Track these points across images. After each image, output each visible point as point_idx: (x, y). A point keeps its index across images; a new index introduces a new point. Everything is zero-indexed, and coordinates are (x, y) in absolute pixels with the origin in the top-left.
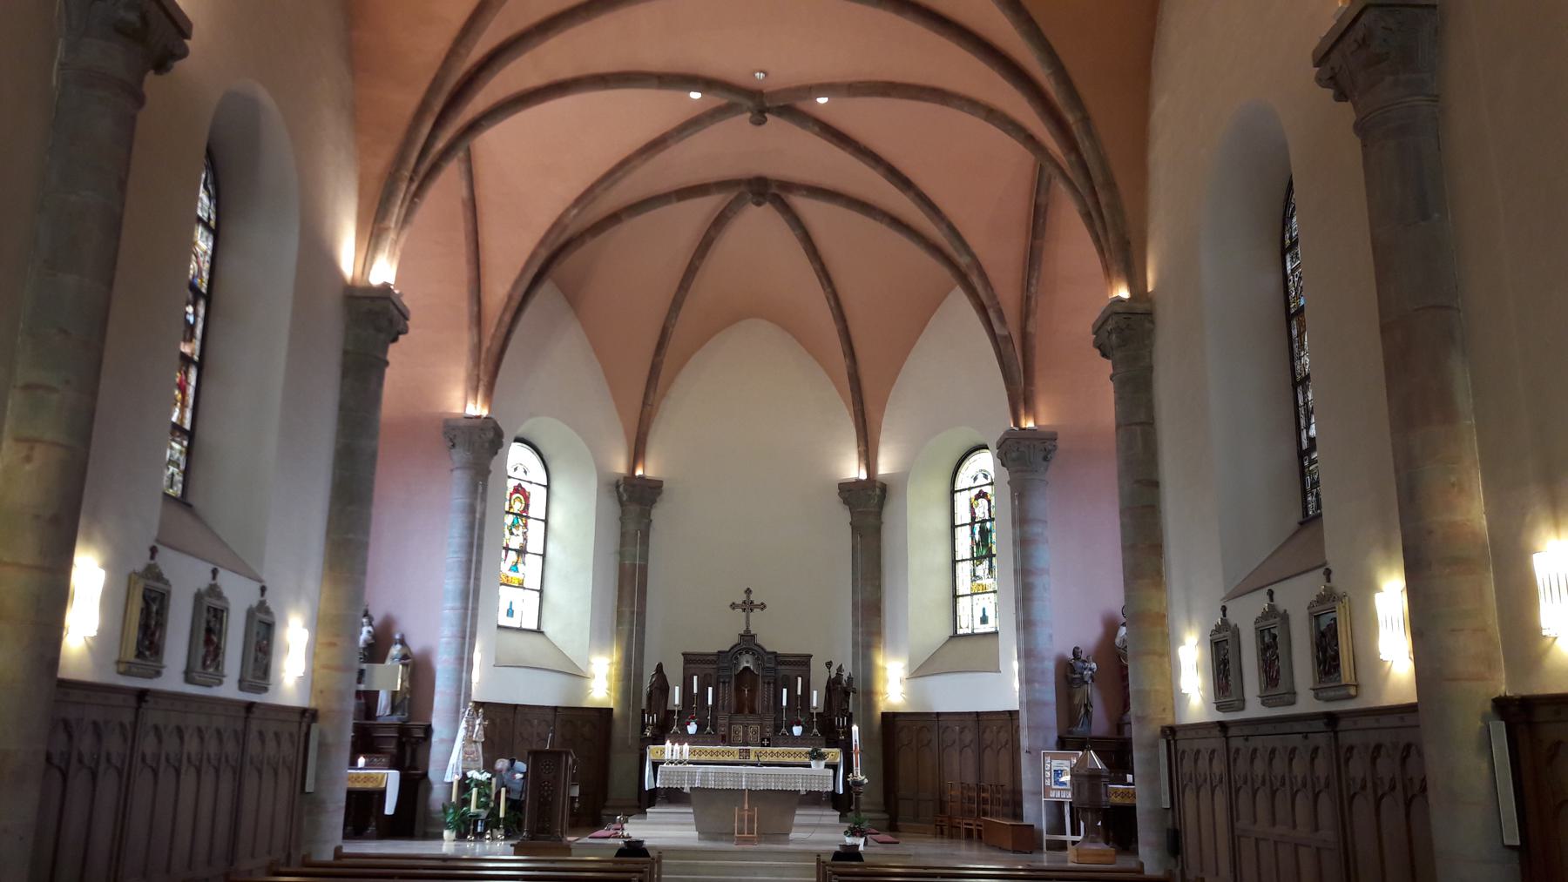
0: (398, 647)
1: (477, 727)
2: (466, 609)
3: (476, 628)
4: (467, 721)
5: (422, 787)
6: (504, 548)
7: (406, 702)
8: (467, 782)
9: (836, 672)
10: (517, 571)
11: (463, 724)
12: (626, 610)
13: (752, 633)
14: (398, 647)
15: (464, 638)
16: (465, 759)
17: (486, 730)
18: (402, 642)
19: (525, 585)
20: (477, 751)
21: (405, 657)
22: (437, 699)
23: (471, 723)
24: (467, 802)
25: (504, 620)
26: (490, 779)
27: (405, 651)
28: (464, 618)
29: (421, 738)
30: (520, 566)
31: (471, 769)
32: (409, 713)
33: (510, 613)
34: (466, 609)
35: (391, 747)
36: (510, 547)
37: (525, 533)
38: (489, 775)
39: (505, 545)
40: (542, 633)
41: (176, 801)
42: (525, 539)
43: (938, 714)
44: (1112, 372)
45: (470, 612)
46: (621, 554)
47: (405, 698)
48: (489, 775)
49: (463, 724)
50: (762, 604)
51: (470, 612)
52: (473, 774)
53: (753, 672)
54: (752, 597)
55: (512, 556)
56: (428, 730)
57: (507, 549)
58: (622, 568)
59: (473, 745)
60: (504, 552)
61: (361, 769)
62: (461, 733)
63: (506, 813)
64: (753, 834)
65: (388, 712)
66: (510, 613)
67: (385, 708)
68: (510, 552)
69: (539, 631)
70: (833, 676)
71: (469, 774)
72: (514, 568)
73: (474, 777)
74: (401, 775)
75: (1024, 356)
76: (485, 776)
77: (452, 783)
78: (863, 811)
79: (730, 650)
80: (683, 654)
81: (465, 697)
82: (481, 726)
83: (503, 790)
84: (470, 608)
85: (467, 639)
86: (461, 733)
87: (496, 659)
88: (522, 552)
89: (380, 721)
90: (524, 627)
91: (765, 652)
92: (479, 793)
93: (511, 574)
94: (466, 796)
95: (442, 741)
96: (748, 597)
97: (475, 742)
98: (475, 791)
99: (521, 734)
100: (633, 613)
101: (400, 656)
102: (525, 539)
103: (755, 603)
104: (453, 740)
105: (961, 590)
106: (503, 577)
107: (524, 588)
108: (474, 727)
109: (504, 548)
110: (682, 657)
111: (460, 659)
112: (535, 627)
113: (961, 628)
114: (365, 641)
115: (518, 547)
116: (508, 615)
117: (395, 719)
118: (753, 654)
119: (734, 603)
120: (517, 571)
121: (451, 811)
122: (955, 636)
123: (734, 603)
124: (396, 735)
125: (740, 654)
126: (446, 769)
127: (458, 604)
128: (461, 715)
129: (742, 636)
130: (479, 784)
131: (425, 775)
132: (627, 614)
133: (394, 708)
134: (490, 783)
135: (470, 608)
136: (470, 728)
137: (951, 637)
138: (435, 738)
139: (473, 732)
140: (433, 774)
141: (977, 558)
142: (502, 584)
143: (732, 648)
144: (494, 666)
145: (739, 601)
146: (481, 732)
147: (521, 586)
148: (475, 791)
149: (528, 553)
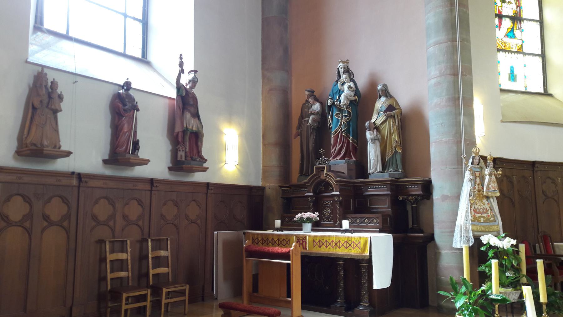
0: (383, 99)
1: (487, 178)
2: (454, 40)
3: (470, 62)
4: (473, 173)
5: (430, 253)
6: (497, 15)
7: (398, 158)
8: (482, 249)
10: (514, 37)
11: (468, 175)
14: (383, 99)
15: (455, 75)
16: (475, 220)
17: (499, 181)
18: (386, 93)
19: (525, 50)
20: (491, 209)
21: (390, 108)
22: (433, 149)
23: (478, 174)
24: (484, 277)
25: (507, 85)
26: (517, 246)
27: (390, 102)
28: (453, 50)
29: (418, 195)
30: (517, 32)
31: (487, 232)
32: (404, 168)
33: (512, 77)
34: (454, 40)
35: (385, 207)
36: (504, 13)
38: (514, 242)
39: (497, 12)
41: (537, 218)
42: (518, 6)
44: (482, 236)
45: (458, 44)
47: (396, 152)
48: (514, 242)
49: (468, 175)
51: (458, 44)
52: (487, 239)
55: (507, 23)
56: (427, 187)
57: (500, 16)
59: (485, 201)
60: (497, 20)
61: (346, 231)
62: (467, 187)
63: (549, 295)
65: (379, 168)
66: (512, 77)
67: (375, 165)
68: (504, 19)
69: (546, 94)
71: (485, 239)
72: (511, 33)
73: (492, 243)
74: (394, 239)
76: (507, 243)
77: (461, 249)
78: (155, 182)
81: (467, 145)
82: (493, 177)
83: (540, 263)
84: (458, 39)
85: (460, 76)
86: (467, 187)
87: (503, 115)
88: (516, 19)
89: (371, 178)
90: (529, 90)
92: (501, 265)
93: (507, 40)
94: (482, 268)
95: (445, 198)
97: (488, 198)
98: (494, 263)
99: (544, 192)
101: (384, 109)
102: (518, 6)
104: (458, 197)
106: (500, 43)
107: (525, 54)
108: (482, 178)
109: (497, 15)
111: (454, 100)
112: (542, 91)
114: (347, 98)
115: (511, 14)
116: (510, 79)
117: (386, 176)
120: (514, 37)
121: (463, 289)
124: (389, 193)
126: (453, 232)
127: (442, 37)
128: (464, 166)
130: (499, 253)
131: (431, 238)
133: (384, 167)
134: (518, 252)
135: (458, 39)
136: (478, 180)
138: (437, 195)
139: (483, 185)
140: (439, 238)
142: (499, 50)
144: (502, 121)
146: (494, 185)
147: (520, 51)
148: (494, 263)
149: (523, 20)
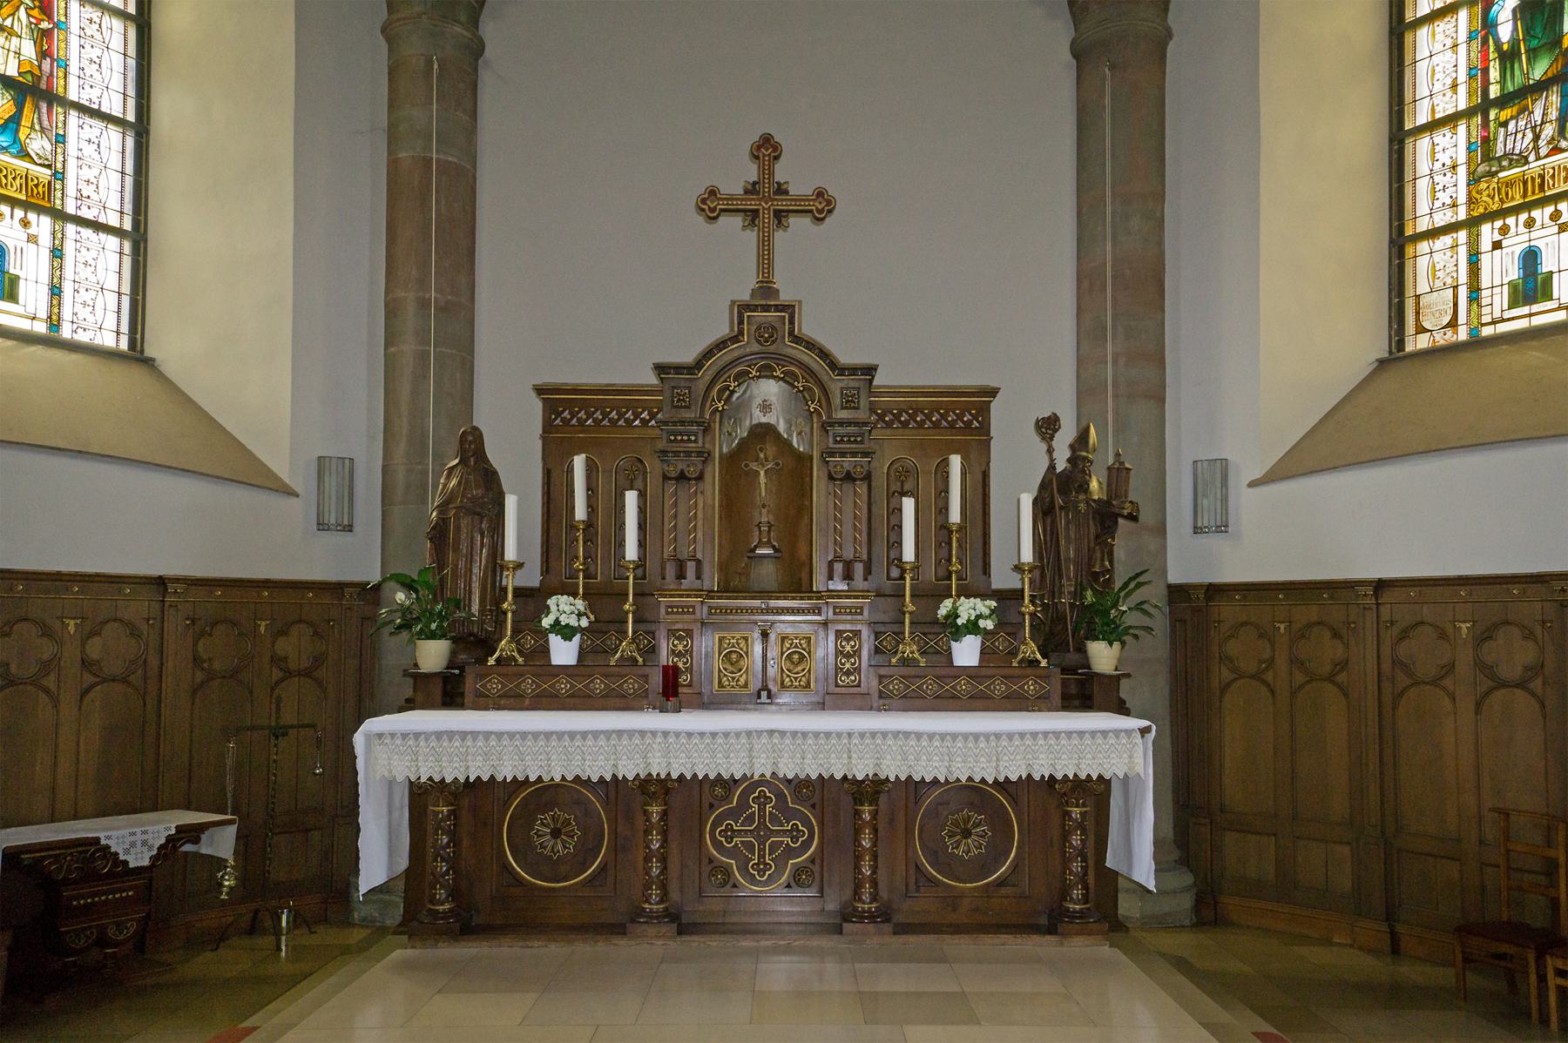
9: (1068, 454)
12: (409, 297)
13: (785, 297)
37: (47, 34)
40: (148, 363)
43: (1381, 585)
46: (393, 137)
50: (820, 194)
53: (788, 444)
54: (781, 173)
58: (393, 165)
64: (784, 316)
69: (136, 355)
70: (1061, 466)
75: (918, 516)
79: (699, 364)
80: (540, 391)
91: (833, 365)
96: (767, 171)
100: (424, 304)
103: (779, 236)
105: (1425, 211)
110: (537, 406)
113: (1421, 330)
118: (789, 378)
119: (713, 193)
122: (1396, 356)
123: (713, 193)
125: (742, 377)
129: (745, 307)
132: (411, 309)
137: (1382, 363)
141: (1503, 101)
143: (708, 354)
145: (732, 185)
